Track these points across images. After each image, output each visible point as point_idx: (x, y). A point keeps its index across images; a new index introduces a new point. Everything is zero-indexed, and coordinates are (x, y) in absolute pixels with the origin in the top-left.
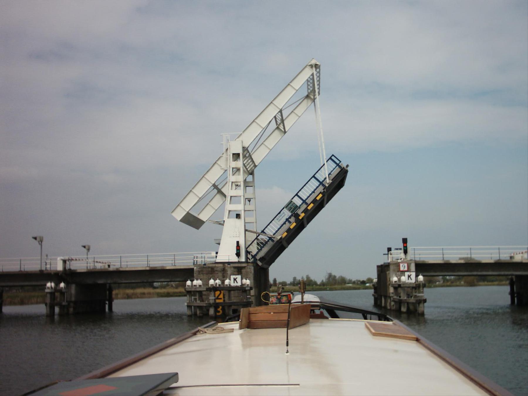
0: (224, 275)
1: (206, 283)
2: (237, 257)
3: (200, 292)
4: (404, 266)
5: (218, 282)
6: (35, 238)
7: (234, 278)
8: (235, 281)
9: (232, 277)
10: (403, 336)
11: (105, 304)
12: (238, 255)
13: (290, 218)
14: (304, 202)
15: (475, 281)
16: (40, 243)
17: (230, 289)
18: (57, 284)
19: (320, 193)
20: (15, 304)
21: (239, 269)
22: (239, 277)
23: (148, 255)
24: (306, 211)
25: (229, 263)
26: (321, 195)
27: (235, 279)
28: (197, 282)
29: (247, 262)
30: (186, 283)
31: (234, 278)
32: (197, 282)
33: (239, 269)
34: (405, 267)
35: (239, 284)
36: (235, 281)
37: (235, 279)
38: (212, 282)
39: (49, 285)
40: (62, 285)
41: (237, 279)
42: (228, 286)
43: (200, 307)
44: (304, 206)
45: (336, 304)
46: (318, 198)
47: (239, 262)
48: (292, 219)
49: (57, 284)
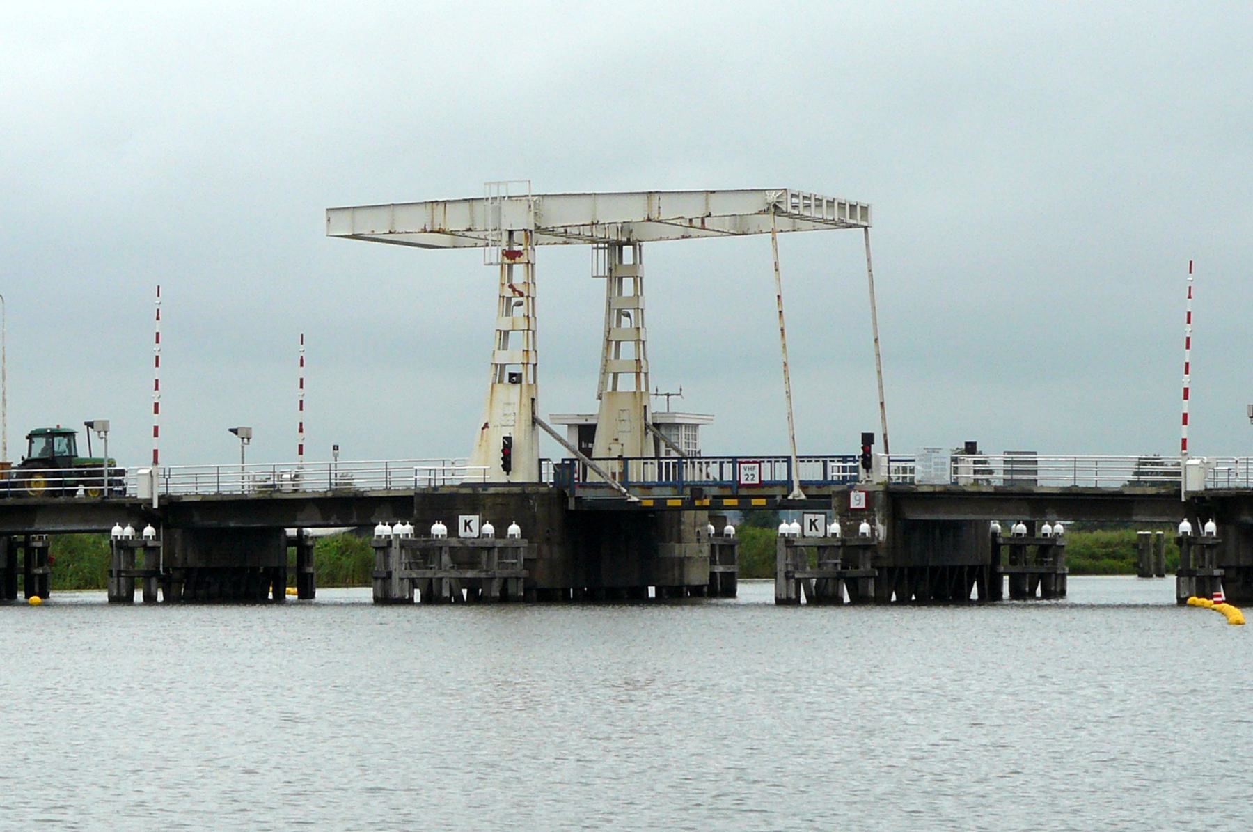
2: (505, 473)
4: (858, 498)
6: (235, 431)
7: (811, 520)
8: (813, 527)
11: (268, 591)
13: (666, 428)
16: (102, 434)
18: (139, 530)
23: (485, 469)
27: (812, 523)
30: (431, 527)
31: (811, 520)
34: (860, 499)
36: (813, 527)
37: (812, 523)
39: (117, 530)
40: (149, 531)
41: (816, 523)
42: (119, 538)
45: (79, 613)
49: (139, 530)
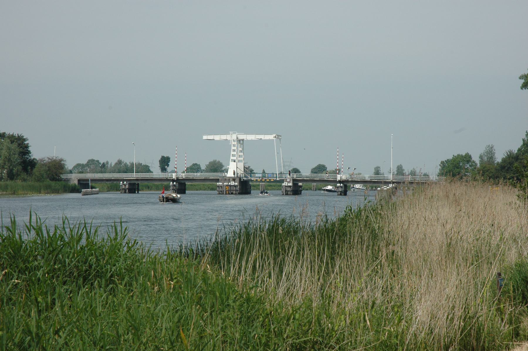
0: (229, 181)
1: (223, 184)
3: (221, 187)
5: (227, 183)
9: (231, 182)
10: (240, 260)
12: (234, 174)
14: (268, 177)
15: (12, 302)
17: (230, 186)
19: (274, 179)
20: (194, 190)
21: (234, 180)
22: (233, 182)
24: (265, 180)
25: (231, 177)
26: (273, 180)
28: (220, 184)
29: (237, 177)
32: (220, 184)
33: (234, 180)
35: (233, 184)
38: (225, 184)
43: (221, 191)
44: (267, 178)
46: (271, 180)
47: (235, 177)
48: (261, 178)
